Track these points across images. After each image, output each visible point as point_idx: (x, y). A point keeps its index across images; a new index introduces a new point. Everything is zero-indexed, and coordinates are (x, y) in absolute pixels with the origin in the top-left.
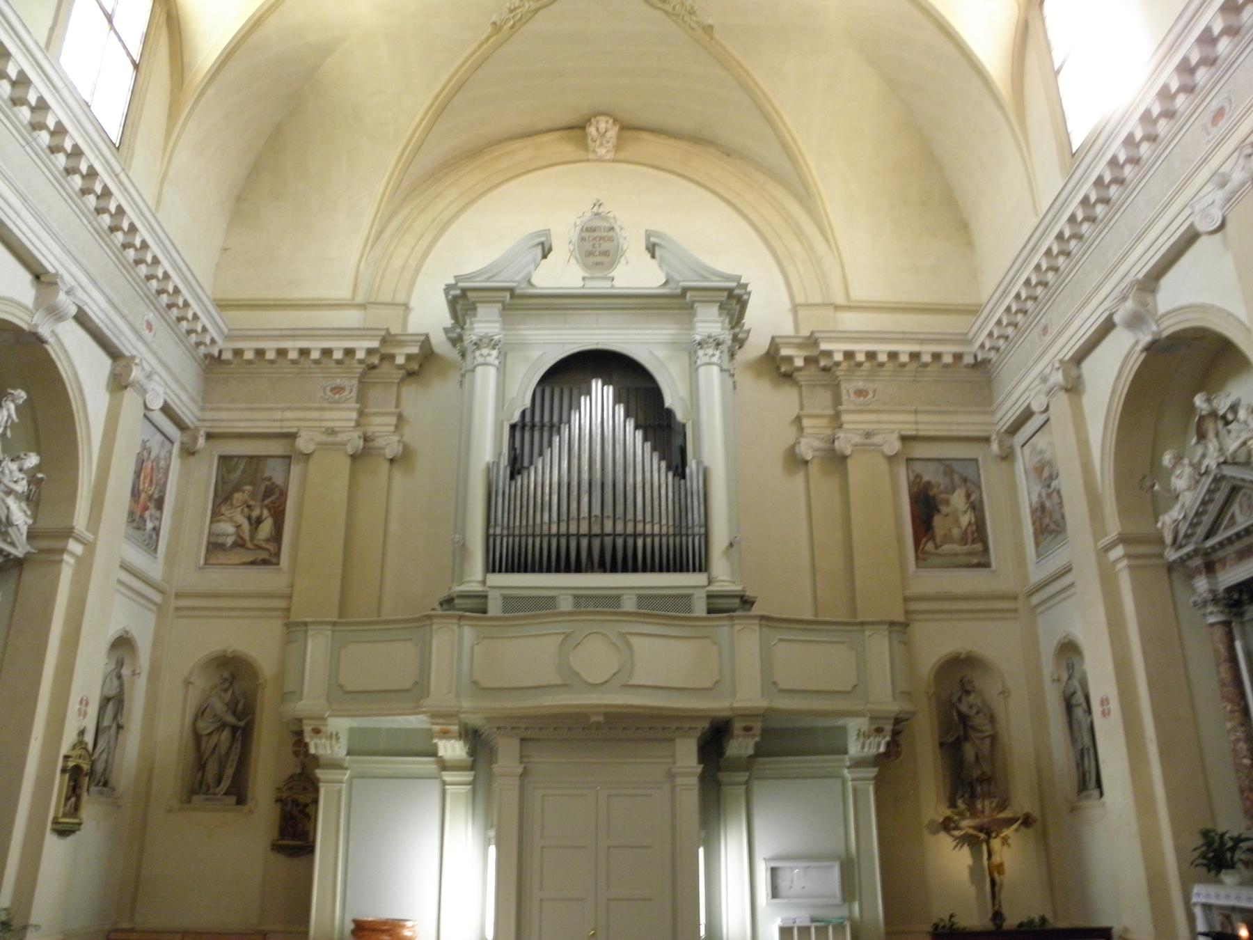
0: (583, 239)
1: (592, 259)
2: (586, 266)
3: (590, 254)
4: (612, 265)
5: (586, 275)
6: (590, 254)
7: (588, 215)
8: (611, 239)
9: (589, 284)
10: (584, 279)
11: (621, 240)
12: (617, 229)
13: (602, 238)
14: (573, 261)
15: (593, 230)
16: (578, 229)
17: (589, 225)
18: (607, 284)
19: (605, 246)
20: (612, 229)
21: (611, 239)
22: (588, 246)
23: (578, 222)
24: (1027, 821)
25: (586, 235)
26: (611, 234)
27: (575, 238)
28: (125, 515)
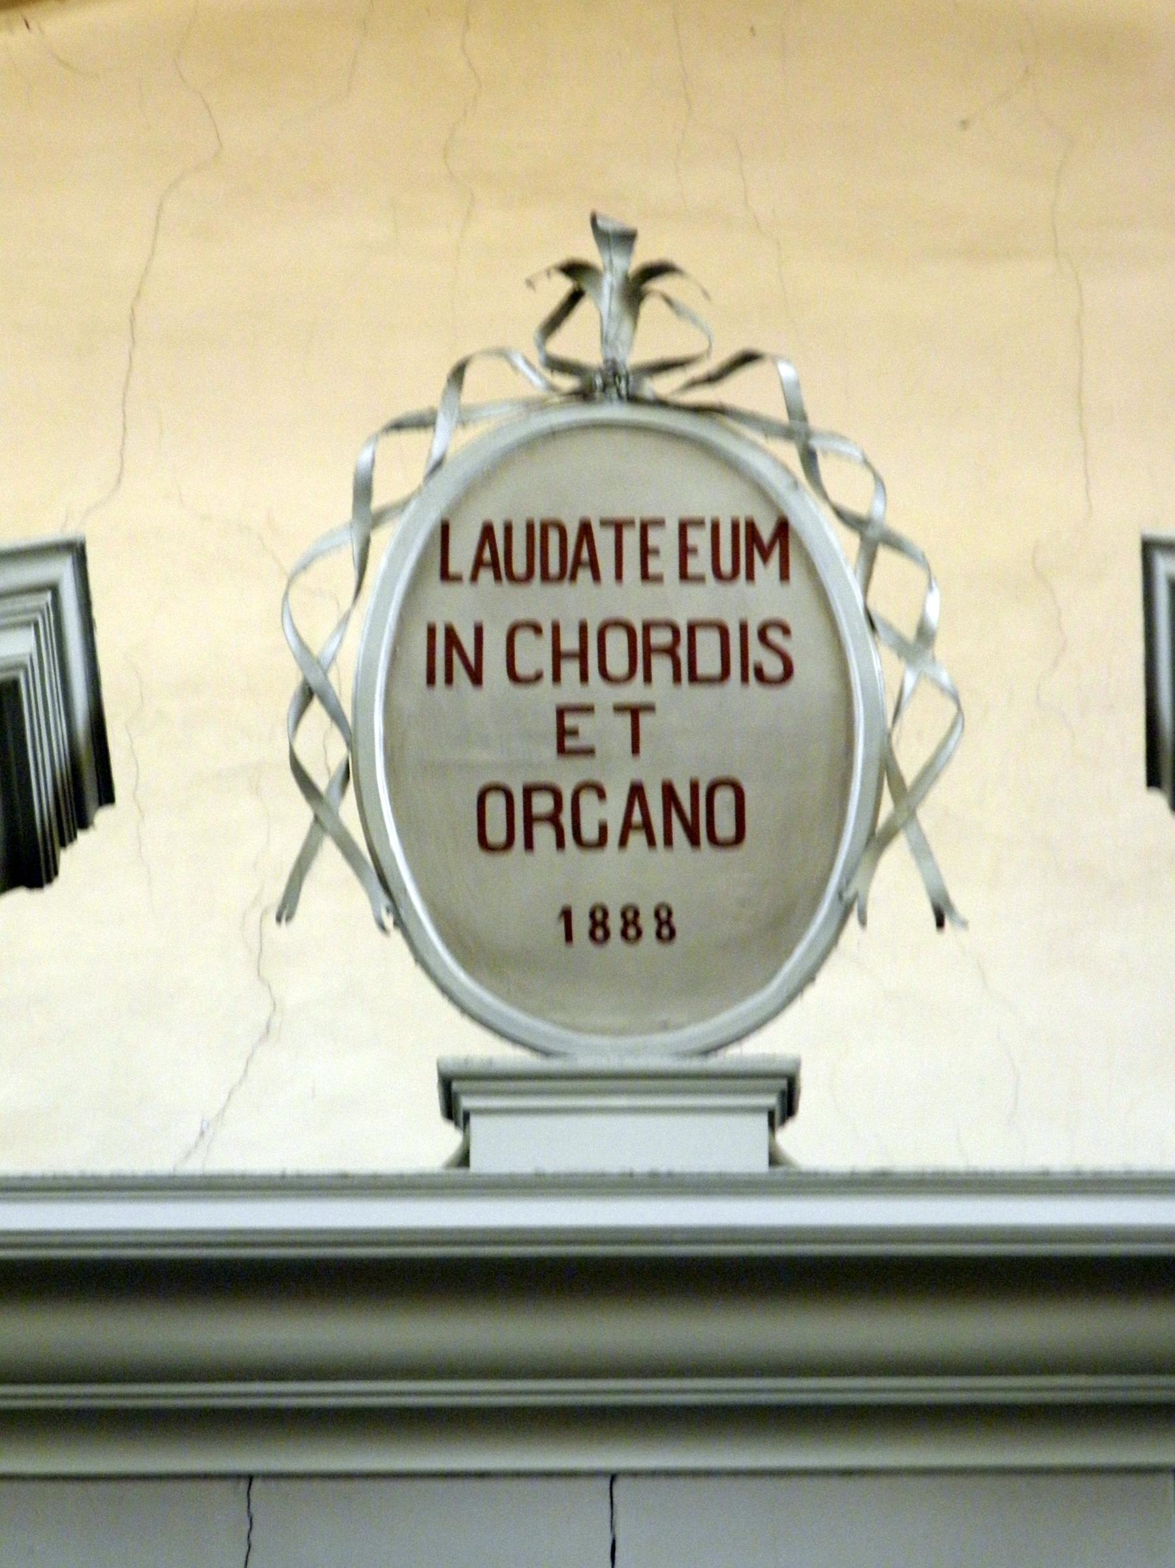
0: (451, 657)
1: (548, 875)
2: (474, 952)
3: (520, 817)
4: (785, 931)
5: (480, 1048)
6: (520, 817)
7: (512, 386)
8: (755, 658)
9: (509, 1141)
10: (454, 1095)
11: (877, 667)
12: (831, 545)
13: (661, 648)
14: (335, 887)
15: (568, 551)
16: (396, 548)
17: (514, 503)
18: (730, 1140)
19: (694, 731)
20: (769, 543)
21: (755, 658)
22: (503, 728)
23: (400, 472)
24: (464, 1159)
25: (467, 605)
26: (763, 596)
27: (355, 637)
28: (644, 934)
